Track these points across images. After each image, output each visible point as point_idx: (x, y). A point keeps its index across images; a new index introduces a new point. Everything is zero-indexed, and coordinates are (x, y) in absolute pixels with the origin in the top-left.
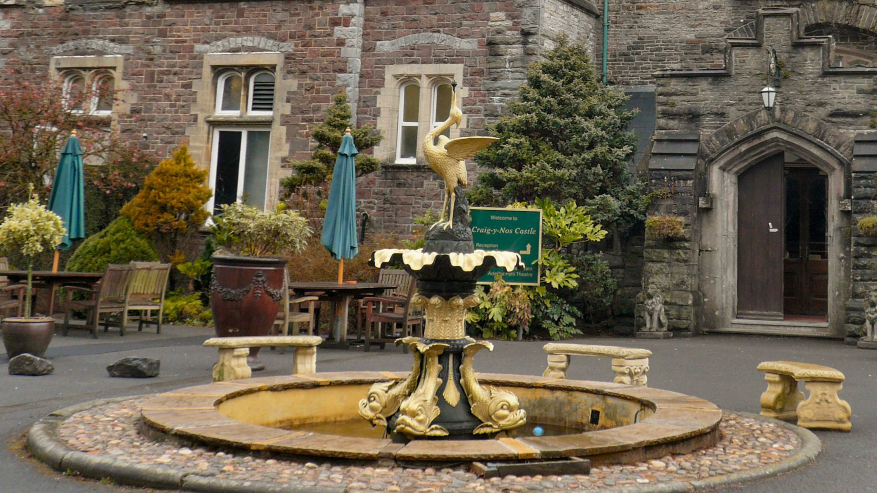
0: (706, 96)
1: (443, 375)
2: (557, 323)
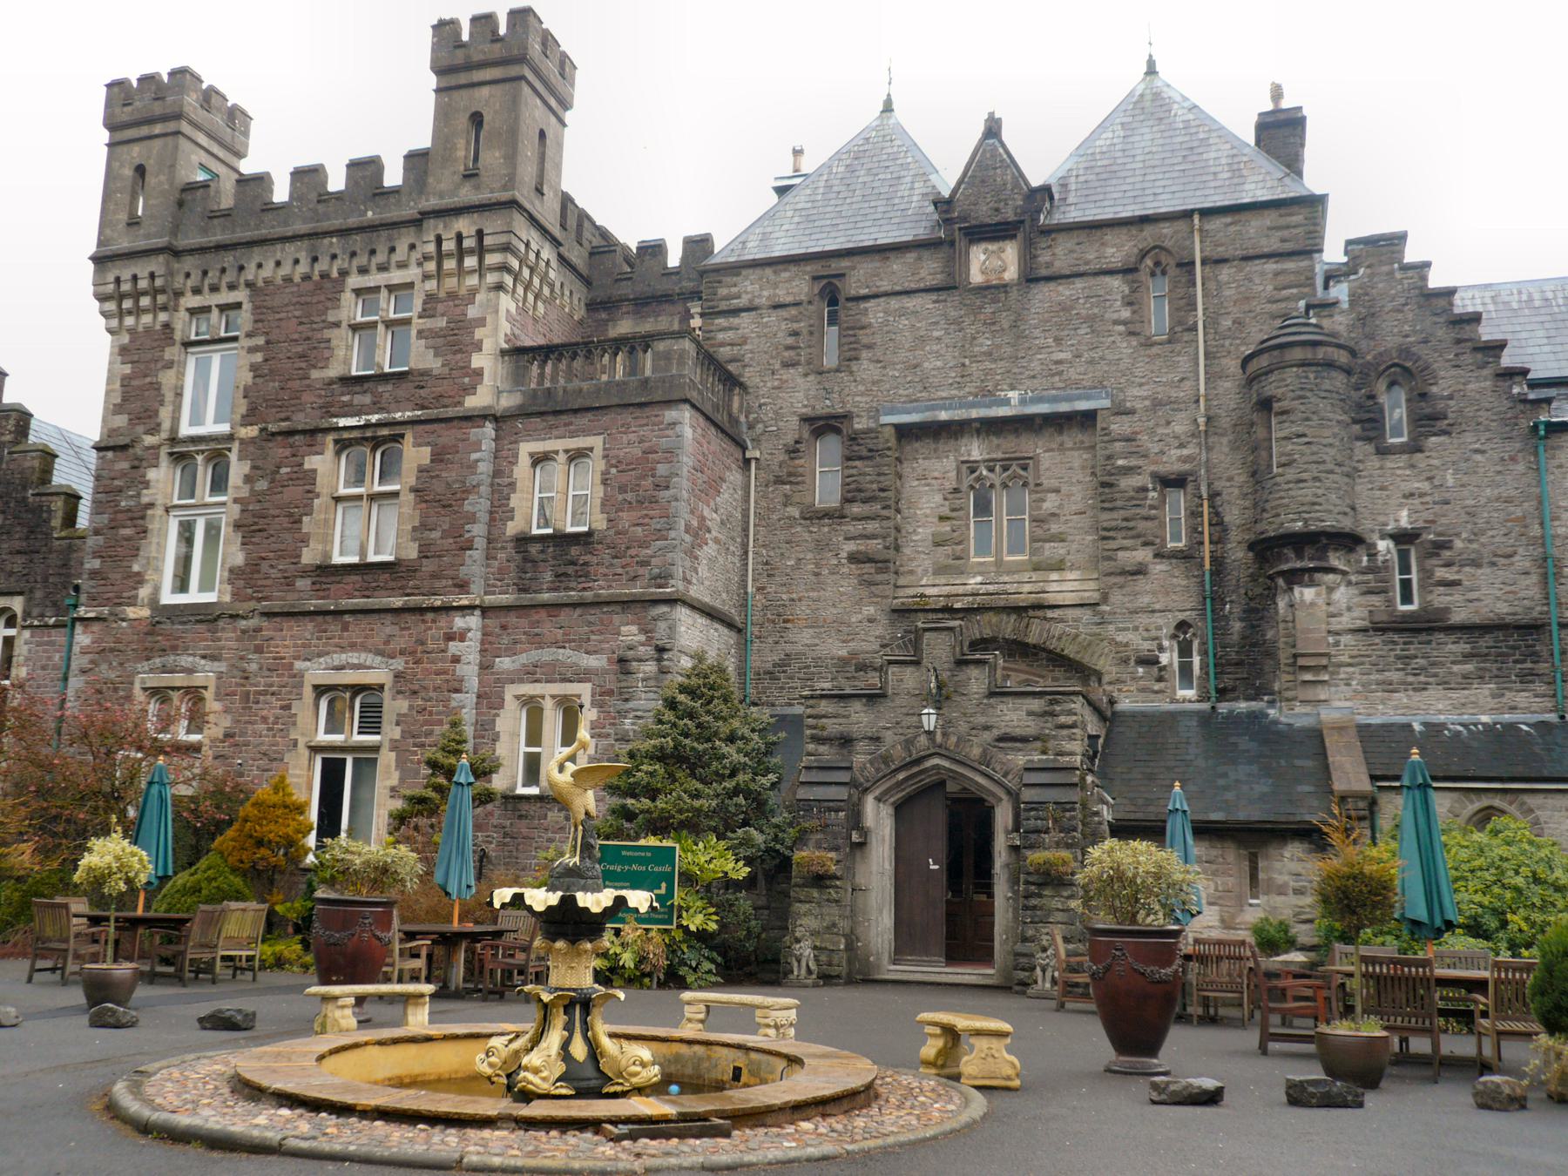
0: (859, 718)
1: (569, 1027)
2: (695, 970)
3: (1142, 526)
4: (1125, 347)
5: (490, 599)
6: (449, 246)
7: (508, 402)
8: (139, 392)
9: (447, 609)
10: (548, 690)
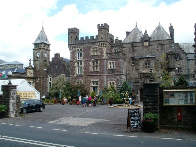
0: (137, 84)
3: (159, 67)
4: (157, 51)
5: (106, 74)
6: (101, 44)
7: (107, 58)
8: (73, 56)
9: (103, 75)
10: (112, 82)
